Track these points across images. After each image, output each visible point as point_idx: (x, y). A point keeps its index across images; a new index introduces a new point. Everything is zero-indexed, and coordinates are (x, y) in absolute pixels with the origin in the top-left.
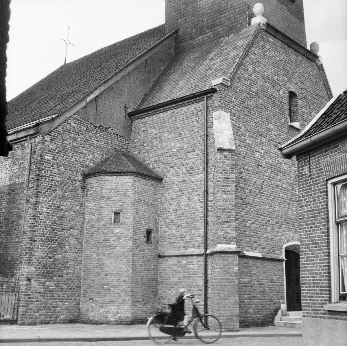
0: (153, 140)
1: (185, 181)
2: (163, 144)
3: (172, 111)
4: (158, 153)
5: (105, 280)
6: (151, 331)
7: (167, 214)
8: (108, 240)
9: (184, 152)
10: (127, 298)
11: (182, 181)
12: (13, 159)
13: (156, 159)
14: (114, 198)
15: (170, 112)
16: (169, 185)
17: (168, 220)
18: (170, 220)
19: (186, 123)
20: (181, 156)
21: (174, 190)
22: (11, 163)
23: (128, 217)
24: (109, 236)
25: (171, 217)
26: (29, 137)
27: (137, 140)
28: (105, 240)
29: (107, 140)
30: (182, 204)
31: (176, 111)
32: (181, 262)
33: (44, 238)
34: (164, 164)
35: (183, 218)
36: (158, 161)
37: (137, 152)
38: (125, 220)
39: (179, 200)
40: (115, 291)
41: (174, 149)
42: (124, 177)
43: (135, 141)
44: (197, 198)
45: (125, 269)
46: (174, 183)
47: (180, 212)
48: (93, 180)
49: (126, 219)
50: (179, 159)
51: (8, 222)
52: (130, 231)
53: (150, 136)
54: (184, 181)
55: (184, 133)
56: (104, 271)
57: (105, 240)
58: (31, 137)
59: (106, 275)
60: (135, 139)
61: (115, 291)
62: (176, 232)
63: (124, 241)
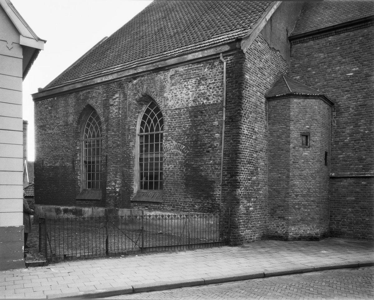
0: (320, 65)
1: (366, 105)
2: (334, 68)
3: (348, 33)
4: (328, 78)
5: (295, 201)
6: (112, 240)
7: (339, 137)
8: (298, 163)
9: (364, 76)
10: (316, 217)
11: (360, 106)
12: (197, 79)
13: (325, 83)
14: (302, 121)
15: (342, 35)
16: (343, 110)
17: (342, 143)
18: (344, 143)
19: (367, 46)
20: (360, 80)
21: (350, 114)
22: (195, 84)
23: (316, 139)
24: (298, 159)
25: (345, 141)
26: (221, 54)
27: (298, 65)
28: (295, 162)
29: (277, 63)
30: (361, 128)
31: (352, 34)
32: (359, 183)
33: (245, 160)
34: (335, 88)
35: (362, 141)
36: (327, 85)
37: (299, 77)
38: (313, 143)
39: (357, 124)
40: (305, 210)
41: (349, 73)
42: (311, 100)
43: (296, 66)
44: (246, 132)
45: (314, 190)
46: (349, 107)
47: (358, 136)
48: (278, 102)
49: (314, 142)
50: (356, 83)
51: (196, 144)
52: (317, 154)
53: (316, 60)
54: (363, 105)
55: (364, 56)
56: (294, 192)
57: (295, 162)
58: (224, 55)
59: (297, 196)
60: (295, 64)
61: (305, 210)
62: (353, 155)
63: (312, 164)
